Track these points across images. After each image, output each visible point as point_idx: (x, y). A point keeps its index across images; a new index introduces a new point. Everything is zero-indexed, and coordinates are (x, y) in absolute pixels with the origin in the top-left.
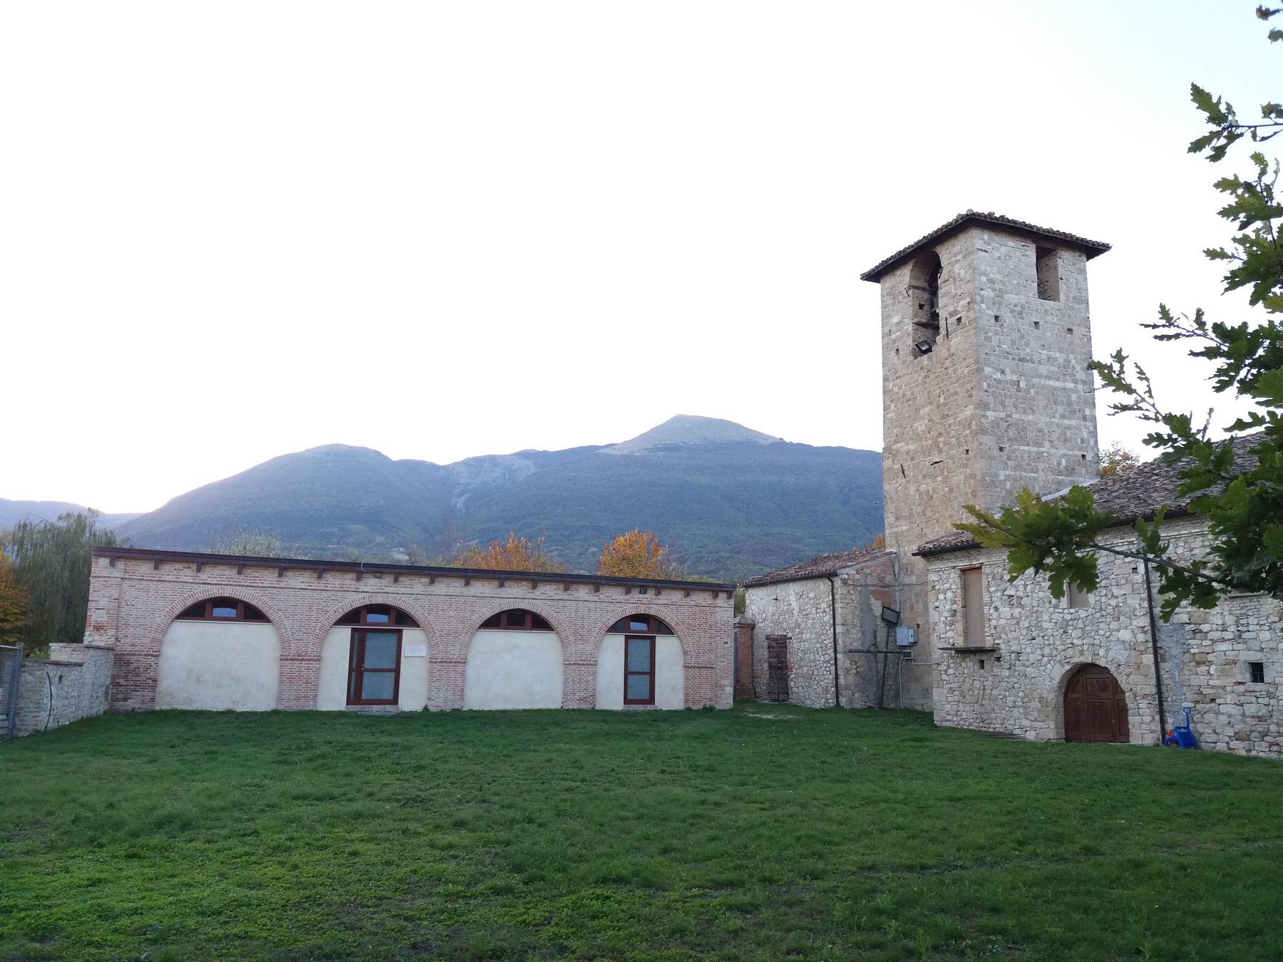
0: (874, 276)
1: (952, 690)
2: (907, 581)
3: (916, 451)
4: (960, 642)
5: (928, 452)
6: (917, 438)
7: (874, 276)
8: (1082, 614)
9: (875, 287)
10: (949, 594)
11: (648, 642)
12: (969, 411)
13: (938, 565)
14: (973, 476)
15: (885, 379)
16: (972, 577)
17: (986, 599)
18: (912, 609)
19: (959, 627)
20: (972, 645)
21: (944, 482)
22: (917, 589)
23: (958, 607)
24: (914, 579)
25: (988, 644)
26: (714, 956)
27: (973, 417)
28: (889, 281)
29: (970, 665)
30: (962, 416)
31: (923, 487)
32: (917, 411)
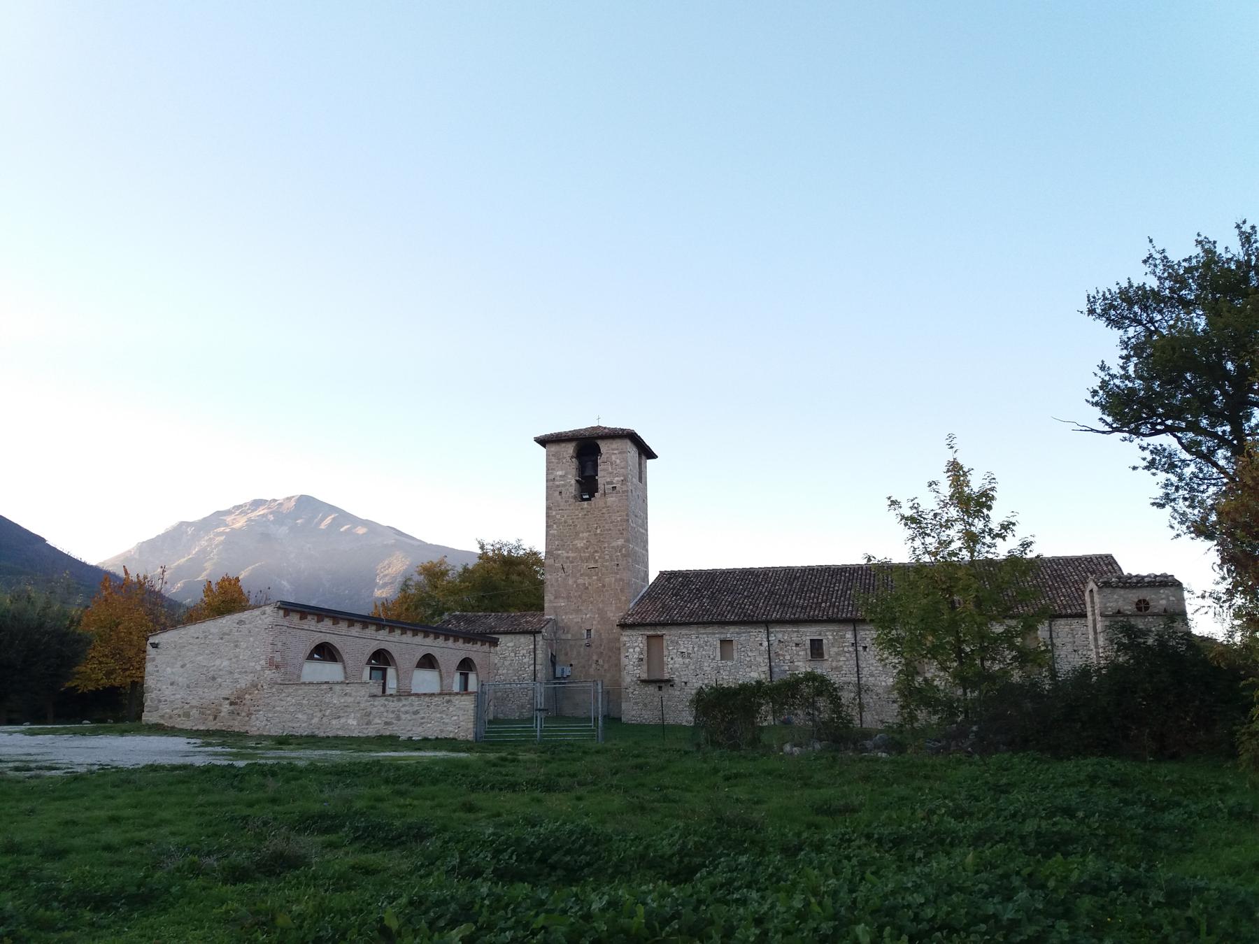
0: (543, 441)
1: (637, 703)
2: (563, 637)
3: (575, 558)
4: (644, 676)
5: (587, 560)
6: (576, 550)
7: (543, 441)
8: (729, 663)
9: (542, 451)
10: (637, 649)
11: (380, 673)
12: (620, 542)
13: (629, 632)
14: (621, 580)
15: (548, 508)
16: (653, 641)
17: (666, 653)
18: (566, 654)
19: (645, 668)
20: (657, 676)
21: (599, 580)
22: (572, 643)
23: (644, 656)
24: (569, 636)
25: (667, 676)
26: (55, 937)
27: (623, 546)
28: (554, 448)
29: (651, 689)
30: (614, 544)
31: (580, 581)
32: (577, 534)
